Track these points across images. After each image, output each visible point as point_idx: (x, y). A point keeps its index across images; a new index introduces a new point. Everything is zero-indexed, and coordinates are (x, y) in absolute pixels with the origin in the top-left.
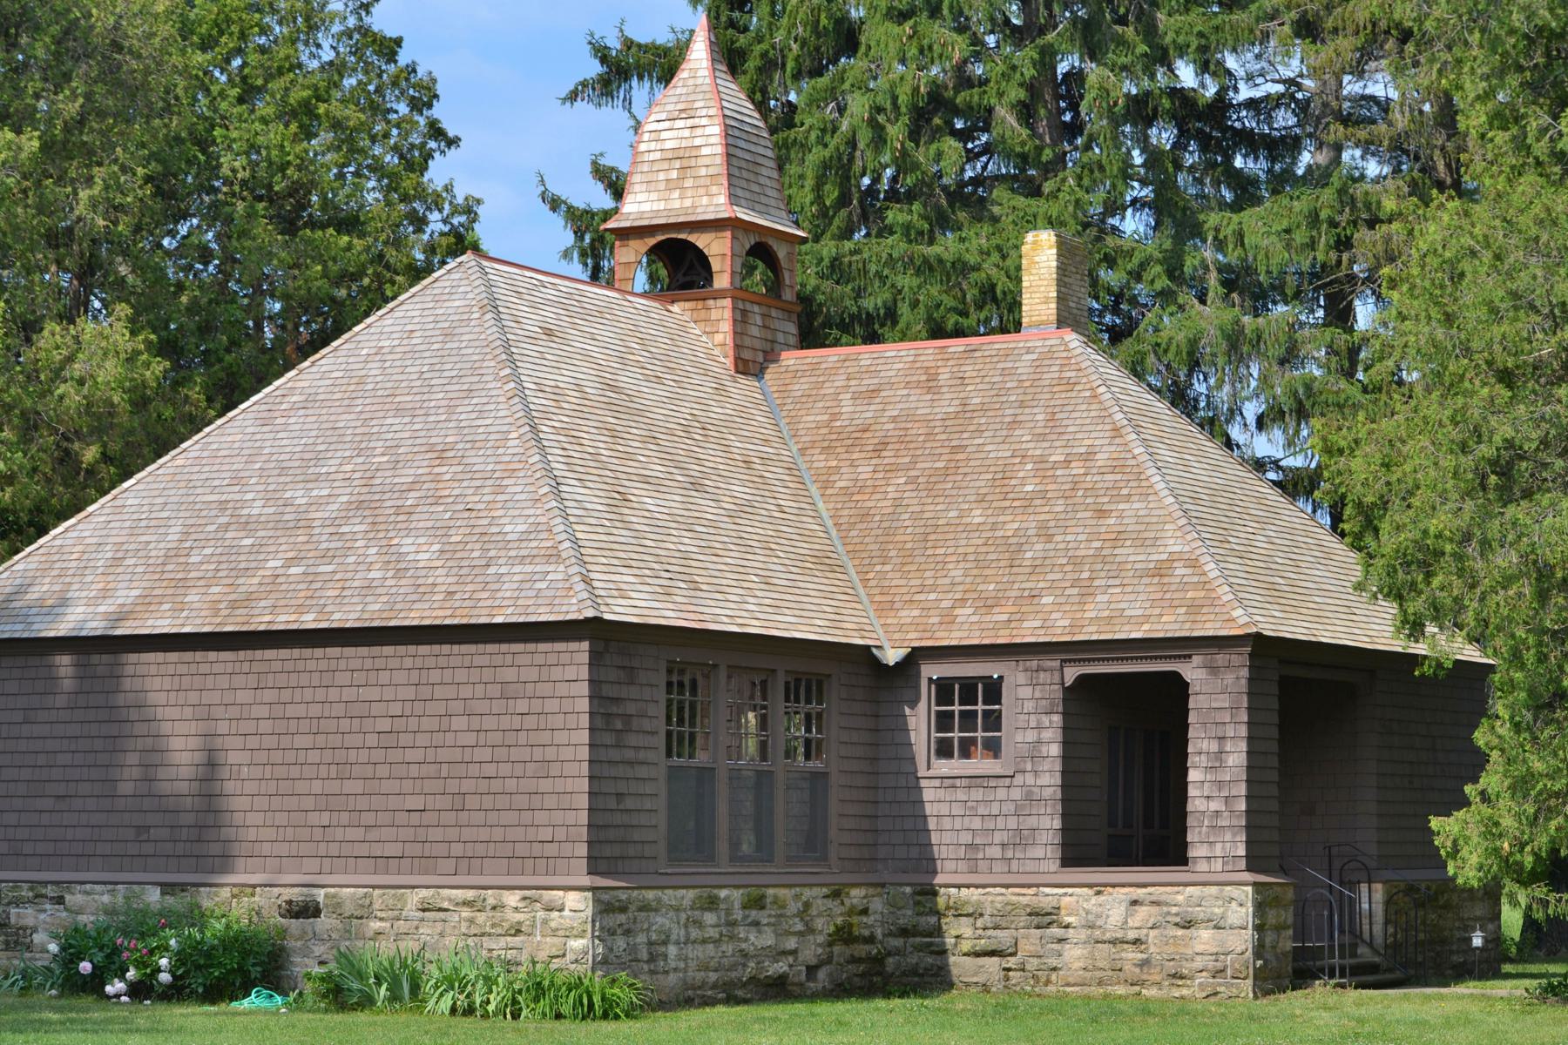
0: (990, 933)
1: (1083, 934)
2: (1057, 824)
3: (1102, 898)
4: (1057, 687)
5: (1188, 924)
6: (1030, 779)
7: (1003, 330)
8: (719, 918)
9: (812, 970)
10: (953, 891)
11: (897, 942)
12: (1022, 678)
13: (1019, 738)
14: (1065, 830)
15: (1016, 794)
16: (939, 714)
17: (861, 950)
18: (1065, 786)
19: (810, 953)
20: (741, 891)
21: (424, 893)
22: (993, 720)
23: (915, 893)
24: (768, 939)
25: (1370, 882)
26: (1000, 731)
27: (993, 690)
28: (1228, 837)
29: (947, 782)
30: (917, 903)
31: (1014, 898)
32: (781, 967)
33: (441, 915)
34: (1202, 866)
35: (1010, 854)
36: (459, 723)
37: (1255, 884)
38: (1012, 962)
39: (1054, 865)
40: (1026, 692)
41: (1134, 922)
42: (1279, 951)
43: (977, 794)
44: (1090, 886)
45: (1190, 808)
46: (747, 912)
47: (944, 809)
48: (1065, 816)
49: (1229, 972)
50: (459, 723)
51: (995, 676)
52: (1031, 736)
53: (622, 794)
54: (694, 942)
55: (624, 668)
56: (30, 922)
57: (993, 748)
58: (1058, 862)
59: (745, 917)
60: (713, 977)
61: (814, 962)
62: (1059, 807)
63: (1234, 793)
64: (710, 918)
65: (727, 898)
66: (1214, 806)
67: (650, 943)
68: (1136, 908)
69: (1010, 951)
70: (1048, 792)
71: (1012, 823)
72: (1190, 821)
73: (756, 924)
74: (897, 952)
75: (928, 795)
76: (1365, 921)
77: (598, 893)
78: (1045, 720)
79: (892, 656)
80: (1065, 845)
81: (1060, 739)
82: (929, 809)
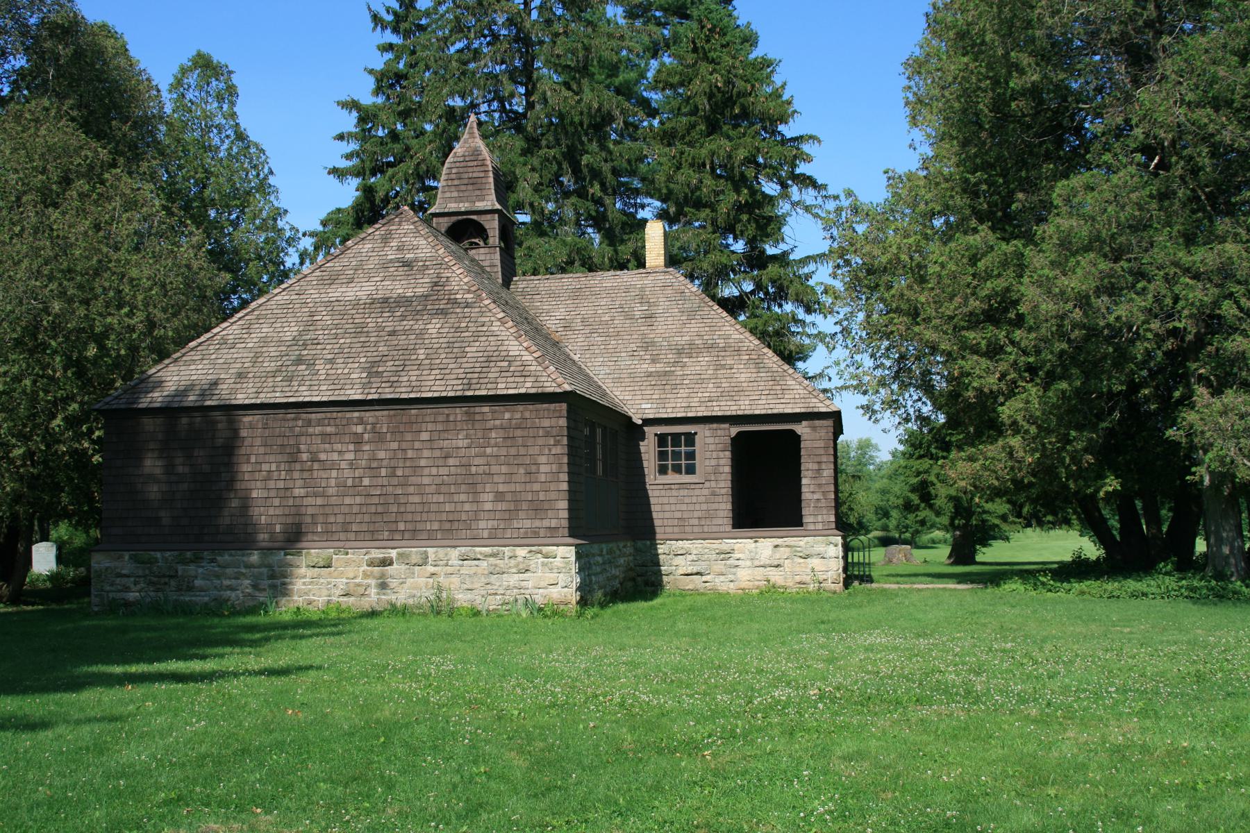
1: (748, 563)
7: (620, 265)
12: (708, 433)
13: (707, 463)
16: (659, 452)
21: (463, 549)
22: (691, 456)
27: (690, 439)
29: (666, 487)
33: (476, 562)
37: (577, 546)
39: (729, 528)
43: (685, 492)
45: (803, 497)
47: (661, 500)
49: (830, 581)
52: (713, 462)
56: (193, 573)
57: (691, 470)
66: (816, 496)
70: (724, 491)
72: (803, 504)
78: (721, 454)
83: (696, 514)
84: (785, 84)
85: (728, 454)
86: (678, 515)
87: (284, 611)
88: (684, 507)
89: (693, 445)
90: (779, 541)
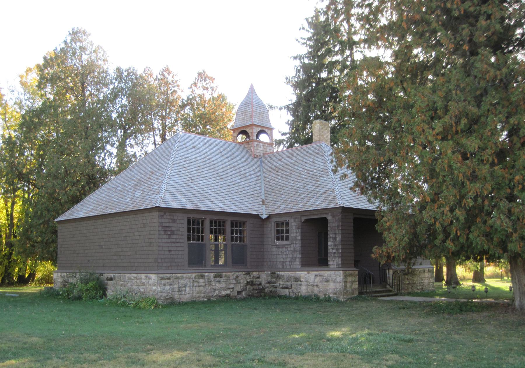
0: (286, 283)
2: (300, 256)
3: (309, 275)
5: (327, 281)
6: (294, 245)
8: (205, 280)
9: (239, 293)
11: (267, 285)
17: (256, 287)
18: (302, 247)
19: (238, 288)
20: (213, 274)
23: (271, 273)
24: (223, 285)
25: (389, 269)
28: (337, 259)
30: (271, 276)
32: (228, 292)
34: (331, 266)
35: (291, 264)
36: (136, 234)
38: (291, 290)
41: (316, 281)
42: (353, 288)
43: (284, 249)
46: (215, 279)
50: (136, 234)
52: (295, 235)
53: (171, 250)
54: (196, 287)
55: (171, 219)
57: (287, 239)
59: (214, 280)
60: (202, 295)
61: (240, 290)
63: (338, 247)
64: (202, 280)
65: (207, 276)
67: (179, 287)
71: (291, 256)
72: (329, 255)
73: (219, 282)
74: (268, 287)
76: (388, 279)
77: (159, 275)
78: (298, 231)
79: (264, 216)
85: (300, 230)
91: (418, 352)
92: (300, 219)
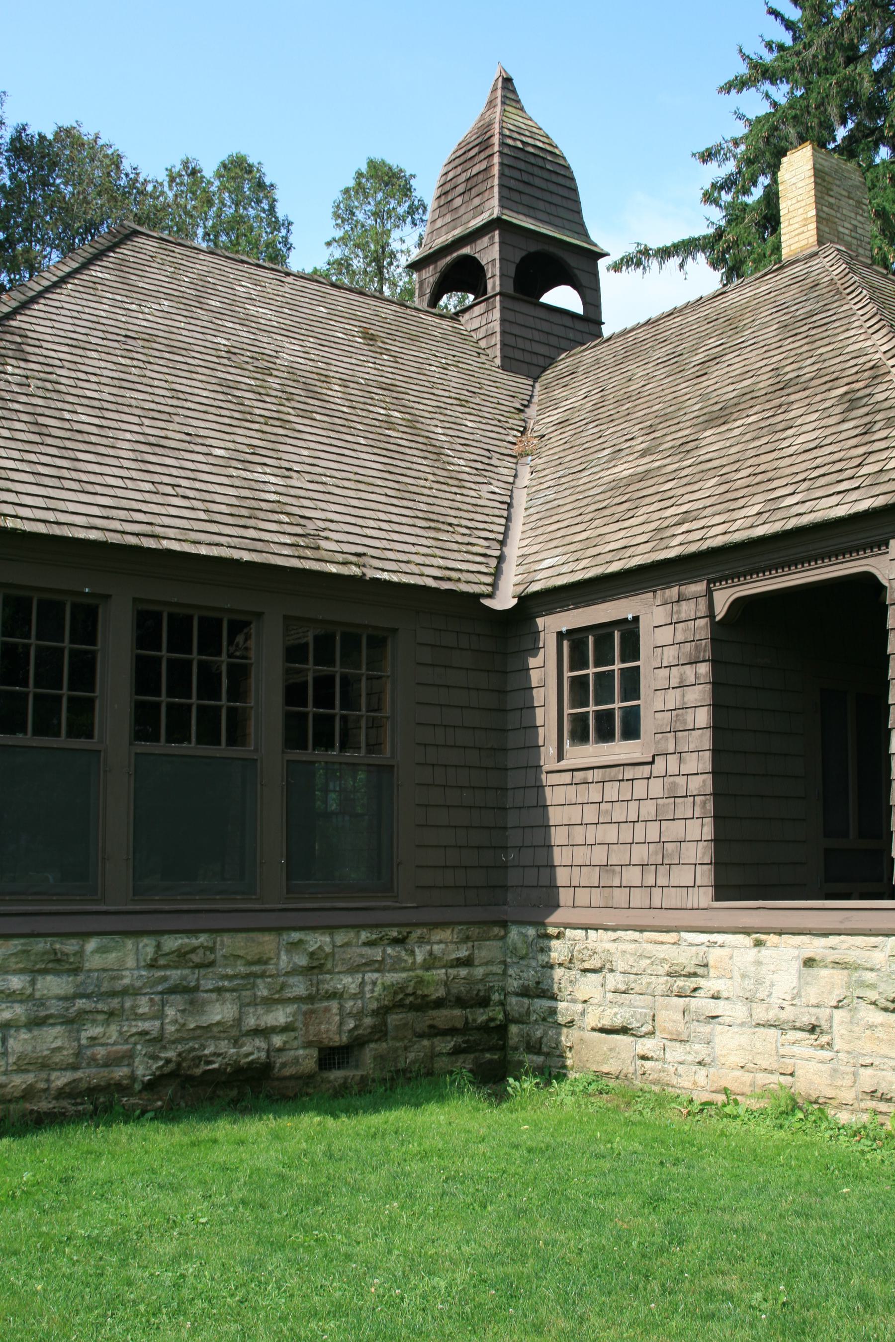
1: (739, 1012)
2: (708, 832)
4: (702, 622)
10: (580, 933)
12: (660, 615)
14: (719, 841)
15: (657, 788)
16: (573, 679)
26: (639, 699)
29: (579, 776)
31: (650, 947)
39: (704, 897)
40: (665, 636)
43: (612, 790)
44: (747, 932)
48: (718, 818)
51: (630, 617)
52: (672, 699)
57: (632, 731)
58: (710, 891)
60: (60, 1080)
62: (710, 806)
68: (814, 971)
69: (644, 1029)
75: (552, 796)
78: (689, 671)
80: (720, 864)
81: (709, 701)
82: (555, 816)
83: (640, 854)
84: (508, 81)
85: (704, 669)
86: (599, 855)
87: (860, 54)
88: (610, 834)
89: (636, 657)
90: (815, 946)
91: (193, 1144)
92: (703, 603)
